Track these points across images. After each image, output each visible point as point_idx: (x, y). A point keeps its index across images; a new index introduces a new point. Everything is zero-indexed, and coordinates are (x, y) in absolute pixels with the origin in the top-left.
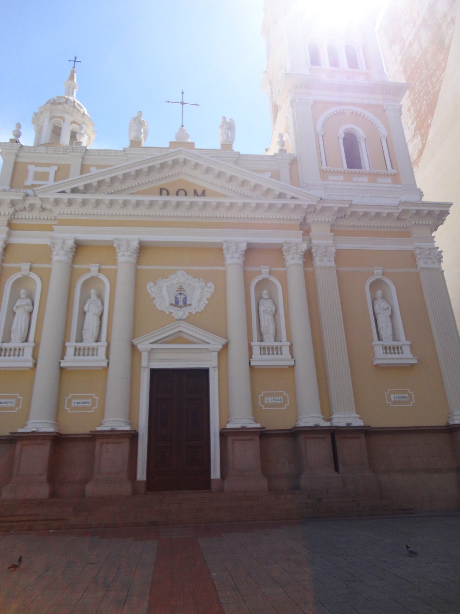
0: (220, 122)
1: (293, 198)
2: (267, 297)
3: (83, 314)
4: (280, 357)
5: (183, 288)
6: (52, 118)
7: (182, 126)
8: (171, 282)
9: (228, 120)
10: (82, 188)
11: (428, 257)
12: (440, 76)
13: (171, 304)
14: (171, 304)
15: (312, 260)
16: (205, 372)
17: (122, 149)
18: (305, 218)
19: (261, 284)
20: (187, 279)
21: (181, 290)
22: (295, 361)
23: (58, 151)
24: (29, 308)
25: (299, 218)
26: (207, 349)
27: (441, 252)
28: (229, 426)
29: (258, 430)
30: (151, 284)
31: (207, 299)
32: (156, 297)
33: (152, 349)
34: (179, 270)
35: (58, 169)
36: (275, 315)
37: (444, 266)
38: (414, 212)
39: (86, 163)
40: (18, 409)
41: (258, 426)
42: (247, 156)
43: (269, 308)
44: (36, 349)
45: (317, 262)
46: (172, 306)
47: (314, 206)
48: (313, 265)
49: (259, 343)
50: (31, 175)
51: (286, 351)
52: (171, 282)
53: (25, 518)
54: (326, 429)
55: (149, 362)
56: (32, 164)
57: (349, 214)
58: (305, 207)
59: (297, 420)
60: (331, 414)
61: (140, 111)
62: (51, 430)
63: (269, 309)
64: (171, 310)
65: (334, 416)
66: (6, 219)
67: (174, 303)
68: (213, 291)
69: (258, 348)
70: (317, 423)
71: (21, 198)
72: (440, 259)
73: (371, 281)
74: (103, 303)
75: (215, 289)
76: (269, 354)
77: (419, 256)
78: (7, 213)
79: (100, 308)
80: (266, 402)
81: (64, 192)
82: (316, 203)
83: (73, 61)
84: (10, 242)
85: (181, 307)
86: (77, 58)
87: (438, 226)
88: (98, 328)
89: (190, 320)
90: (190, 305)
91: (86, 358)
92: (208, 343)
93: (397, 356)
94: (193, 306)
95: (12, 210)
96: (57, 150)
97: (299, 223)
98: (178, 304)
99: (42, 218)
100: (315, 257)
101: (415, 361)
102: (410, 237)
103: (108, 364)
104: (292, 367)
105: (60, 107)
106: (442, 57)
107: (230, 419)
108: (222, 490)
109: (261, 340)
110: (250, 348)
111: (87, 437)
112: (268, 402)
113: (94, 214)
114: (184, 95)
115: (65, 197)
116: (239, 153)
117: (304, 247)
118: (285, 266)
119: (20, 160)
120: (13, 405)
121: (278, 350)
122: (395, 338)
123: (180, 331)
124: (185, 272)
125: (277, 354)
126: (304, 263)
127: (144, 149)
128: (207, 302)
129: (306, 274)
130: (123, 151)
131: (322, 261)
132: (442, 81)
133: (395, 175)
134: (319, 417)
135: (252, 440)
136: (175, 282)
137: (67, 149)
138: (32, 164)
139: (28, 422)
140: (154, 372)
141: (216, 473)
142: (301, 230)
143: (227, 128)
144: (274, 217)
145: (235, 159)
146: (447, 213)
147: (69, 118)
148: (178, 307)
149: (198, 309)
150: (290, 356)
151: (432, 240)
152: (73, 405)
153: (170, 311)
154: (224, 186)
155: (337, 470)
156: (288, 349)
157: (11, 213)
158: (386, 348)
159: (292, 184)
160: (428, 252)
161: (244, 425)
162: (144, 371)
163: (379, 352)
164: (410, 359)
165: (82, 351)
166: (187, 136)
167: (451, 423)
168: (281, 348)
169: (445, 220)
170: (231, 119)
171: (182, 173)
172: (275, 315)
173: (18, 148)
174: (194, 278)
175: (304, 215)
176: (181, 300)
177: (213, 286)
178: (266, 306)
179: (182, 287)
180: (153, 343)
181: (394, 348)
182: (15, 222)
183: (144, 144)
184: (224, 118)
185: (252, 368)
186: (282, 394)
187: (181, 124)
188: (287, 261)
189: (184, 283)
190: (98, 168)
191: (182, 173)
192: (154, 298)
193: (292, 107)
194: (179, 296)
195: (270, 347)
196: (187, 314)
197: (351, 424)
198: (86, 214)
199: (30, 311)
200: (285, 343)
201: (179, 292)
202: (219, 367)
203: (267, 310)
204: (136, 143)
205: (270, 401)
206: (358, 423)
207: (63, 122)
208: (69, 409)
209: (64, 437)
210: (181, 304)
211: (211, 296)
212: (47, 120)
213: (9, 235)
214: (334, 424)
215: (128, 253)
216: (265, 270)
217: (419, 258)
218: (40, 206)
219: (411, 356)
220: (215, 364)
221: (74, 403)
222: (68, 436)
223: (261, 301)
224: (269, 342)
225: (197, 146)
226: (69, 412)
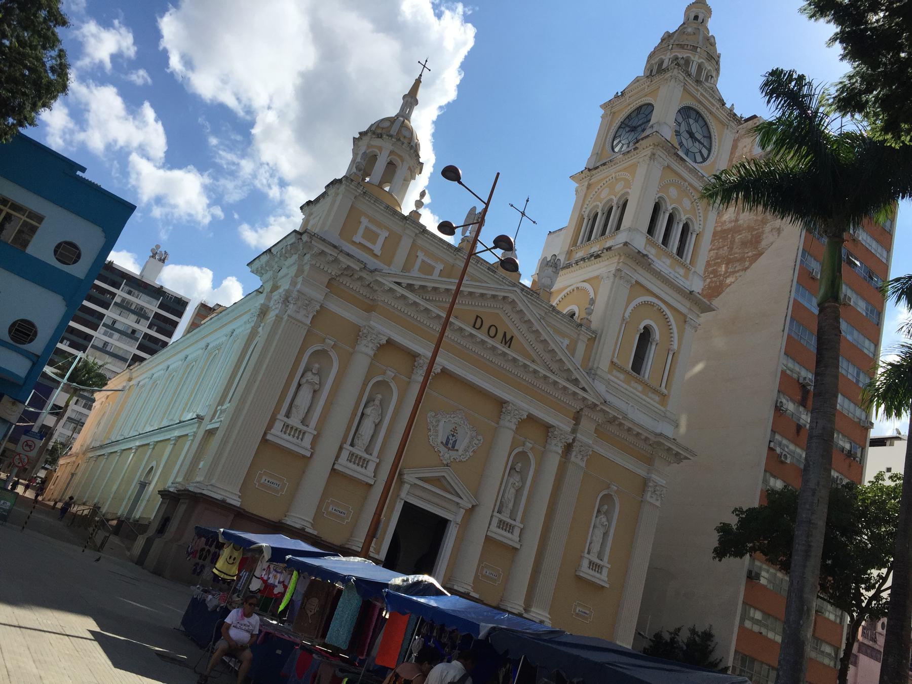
1: (584, 389)
13: (442, 443)
16: (443, 523)
18: (581, 409)
19: (382, 385)
22: (521, 545)
26: (458, 504)
41: (315, 533)
44: (315, 439)
47: (596, 405)
51: (372, 467)
57: (356, 276)
62: (238, 504)
67: (444, 442)
73: (315, 349)
81: (399, 284)
85: (449, 449)
93: (359, 469)
94: (460, 452)
101: (607, 586)
103: (312, 454)
107: (289, 513)
109: (288, 415)
116: (425, 227)
118: (354, 348)
121: (364, 463)
122: (368, 450)
123: (444, 477)
140: (408, 508)
144: (456, 340)
150: (519, 539)
158: (501, 521)
163: (585, 563)
164: (603, 581)
168: (304, 433)
176: (451, 442)
180: (420, 479)
181: (360, 458)
194: (450, 437)
195: (359, 457)
200: (311, 429)
206: (235, 501)
210: (450, 446)
219: (606, 579)
220: (459, 520)
224: (295, 421)
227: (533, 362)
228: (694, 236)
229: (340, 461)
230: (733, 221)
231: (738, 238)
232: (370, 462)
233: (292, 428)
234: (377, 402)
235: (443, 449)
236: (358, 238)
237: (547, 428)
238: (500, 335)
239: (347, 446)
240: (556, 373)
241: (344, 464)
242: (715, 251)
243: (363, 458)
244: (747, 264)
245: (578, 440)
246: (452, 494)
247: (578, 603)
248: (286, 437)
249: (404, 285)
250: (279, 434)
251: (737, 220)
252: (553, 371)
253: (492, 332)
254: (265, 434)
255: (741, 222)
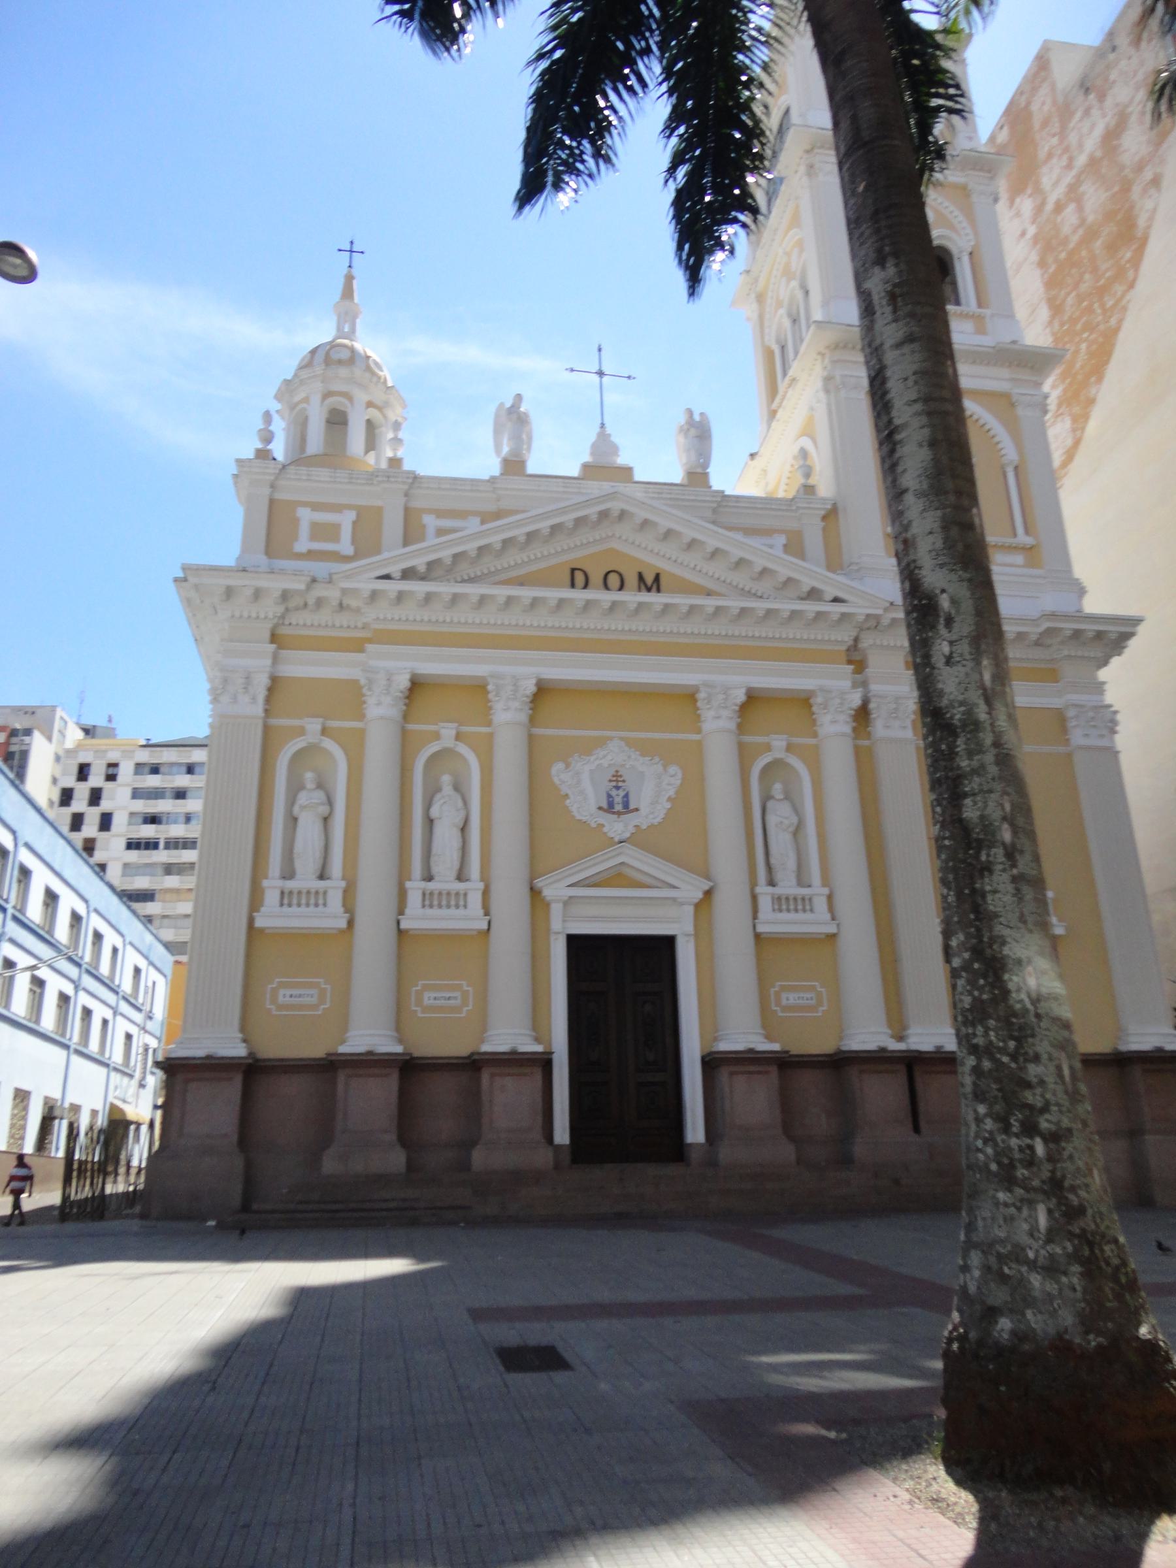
0: (682, 419)
1: (836, 600)
2: (782, 797)
3: (430, 822)
4: (808, 916)
5: (621, 776)
6: (327, 395)
7: (603, 425)
8: (597, 762)
9: (697, 418)
10: (422, 569)
11: (1092, 723)
12: (1123, 296)
13: (600, 808)
14: (600, 808)
15: (867, 726)
16: (669, 942)
17: (487, 478)
20: (629, 757)
21: (617, 780)
22: (838, 925)
23: (358, 479)
24: (324, 810)
25: (846, 639)
26: (674, 899)
27: (1116, 712)
28: (723, 1046)
29: (539, 1057)
30: (560, 766)
31: (669, 799)
32: (569, 792)
33: (571, 897)
34: (611, 739)
35: (358, 515)
36: (797, 831)
37: (1122, 741)
38: (1068, 633)
39: (415, 504)
40: (324, 1009)
41: (776, 1047)
42: (738, 498)
43: (786, 818)
44: (349, 895)
45: (879, 728)
46: (601, 812)
47: (877, 618)
48: (869, 733)
49: (770, 889)
50: (304, 530)
51: (821, 904)
52: (597, 762)
53: (392, 1205)
54: (905, 1054)
55: (564, 921)
56: (305, 504)
58: (861, 618)
59: (841, 1039)
60: (904, 1027)
61: (519, 395)
63: (786, 822)
64: (601, 821)
65: (910, 1032)
66: (269, 625)
67: (605, 805)
68: (679, 782)
69: (769, 899)
70: (882, 1044)
71: (302, 587)
72: (1111, 726)
74: (465, 803)
75: (684, 779)
76: (788, 910)
77: (1074, 723)
78: (271, 615)
79: (463, 814)
80: (784, 1002)
81: (387, 577)
82: (880, 612)
83: (351, 258)
84: (277, 675)
85: (619, 813)
86: (356, 242)
87: (1111, 657)
88: (461, 852)
89: (638, 839)
90: (637, 810)
91: (444, 912)
92: (674, 887)
93: (800, 916)
94: (644, 811)
95: (280, 610)
96: (354, 476)
97: (844, 648)
98: (613, 808)
99: (338, 624)
100: (874, 719)
102: (1057, 682)
104: (832, 937)
105: (343, 372)
106: (1128, 255)
108: (711, 1162)
110: (754, 898)
111: (462, 1064)
112: (789, 1002)
113: (444, 622)
114: (603, 352)
115: (392, 587)
116: (723, 492)
117: (856, 700)
119: (279, 496)
120: (314, 1000)
121: (803, 904)
123: (622, 864)
124: (623, 743)
125: (804, 910)
126: (854, 729)
127: (531, 479)
128: (668, 805)
129: (857, 751)
130: (488, 481)
131: (888, 727)
132: (1125, 309)
133: (1031, 548)
134: (885, 1033)
135: (767, 1072)
136: (605, 763)
137: (377, 476)
138: (305, 504)
139: (348, 1035)
140: (574, 942)
141: (695, 1131)
142: (850, 662)
143: (697, 437)
145: (715, 505)
146: (1129, 636)
147: (361, 397)
148: (614, 813)
149: (654, 818)
151: (1099, 687)
152: (426, 1002)
153: (598, 822)
154: (698, 568)
155: (917, 1129)
156: (823, 900)
157: (279, 615)
159: (830, 567)
160: (1091, 714)
161: (752, 1046)
162: (556, 939)
165: (436, 897)
166: (614, 450)
167: (1123, 1048)
168: (325, 893)
169: (1124, 647)
170: (702, 414)
171: (613, 535)
172: (797, 831)
173: (277, 471)
174: (643, 755)
175: (854, 634)
176: (618, 800)
177: (680, 775)
178: (780, 815)
179: (619, 774)
182: (284, 631)
183: (532, 468)
184: (690, 412)
185: (757, 936)
186: (813, 988)
187: (600, 422)
188: (822, 725)
189: (623, 766)
190: (438, 516)
191: (613, 535)
192: (567, 795)
193: (827, 391)
194: (614, 793)
196: (631, 829)
197: (942, 1047)
198: (430, 621)
199: (326, 814)
201: (614, 784)
202: (697, 935)
203: (781, 822)
204: (514, 465)
205: (791, 1001)
207: (349, 405)
208: (465, 1009)
209: (262, 1064)
211: (677, 793)
212: (316, 399)
213: (275, 659)
214: (914, 1047)
215: (516, 704)
216: (779, 743)
217: (1075, 726)
218: (338, 602)
220: (690, 928)
221: (428, 998)
222: (267, 1063)
223: (770, 804)
224: (787, 886)
225: (639, 476)
226: (420, 1015)
227: (708, 595)
228: (966, 259)
229: (761, 915)
230: (1079, 226)
231: (1098, 244)
232: (331, 893)
233: (300, 893)
234: (447, 789)
235: (606, 820)
236: (303, 544)
237: (803, 702)
238: (631, 580)
239: (763, 889)
240: (765, 596)
241: (772, 922)
242: (1074, 294)
243: (791, 898)
244: (1131, 274)
245: (875, 696)
246: (657, 887)
247: (776, 1006)
248: (435, 912)
249: (397, 575)
250: (420, 911)
251: (1083, 221)
252: (759, 594)
253: (614, 580)
254: (251, 921)
255: (1091, 218)
